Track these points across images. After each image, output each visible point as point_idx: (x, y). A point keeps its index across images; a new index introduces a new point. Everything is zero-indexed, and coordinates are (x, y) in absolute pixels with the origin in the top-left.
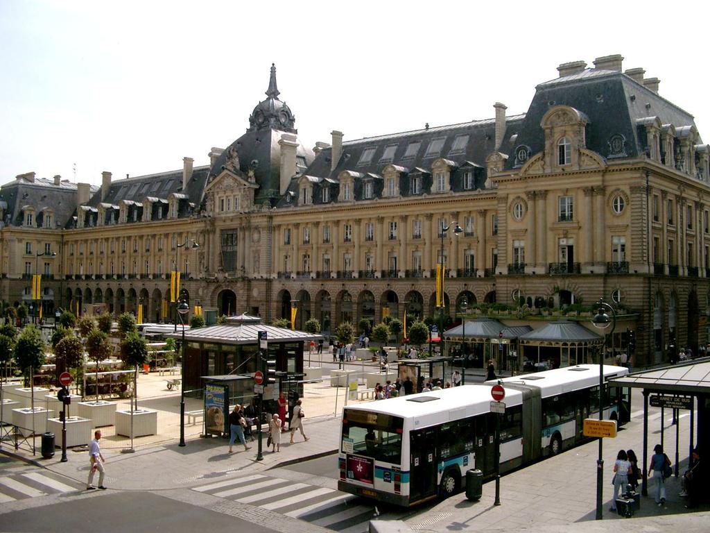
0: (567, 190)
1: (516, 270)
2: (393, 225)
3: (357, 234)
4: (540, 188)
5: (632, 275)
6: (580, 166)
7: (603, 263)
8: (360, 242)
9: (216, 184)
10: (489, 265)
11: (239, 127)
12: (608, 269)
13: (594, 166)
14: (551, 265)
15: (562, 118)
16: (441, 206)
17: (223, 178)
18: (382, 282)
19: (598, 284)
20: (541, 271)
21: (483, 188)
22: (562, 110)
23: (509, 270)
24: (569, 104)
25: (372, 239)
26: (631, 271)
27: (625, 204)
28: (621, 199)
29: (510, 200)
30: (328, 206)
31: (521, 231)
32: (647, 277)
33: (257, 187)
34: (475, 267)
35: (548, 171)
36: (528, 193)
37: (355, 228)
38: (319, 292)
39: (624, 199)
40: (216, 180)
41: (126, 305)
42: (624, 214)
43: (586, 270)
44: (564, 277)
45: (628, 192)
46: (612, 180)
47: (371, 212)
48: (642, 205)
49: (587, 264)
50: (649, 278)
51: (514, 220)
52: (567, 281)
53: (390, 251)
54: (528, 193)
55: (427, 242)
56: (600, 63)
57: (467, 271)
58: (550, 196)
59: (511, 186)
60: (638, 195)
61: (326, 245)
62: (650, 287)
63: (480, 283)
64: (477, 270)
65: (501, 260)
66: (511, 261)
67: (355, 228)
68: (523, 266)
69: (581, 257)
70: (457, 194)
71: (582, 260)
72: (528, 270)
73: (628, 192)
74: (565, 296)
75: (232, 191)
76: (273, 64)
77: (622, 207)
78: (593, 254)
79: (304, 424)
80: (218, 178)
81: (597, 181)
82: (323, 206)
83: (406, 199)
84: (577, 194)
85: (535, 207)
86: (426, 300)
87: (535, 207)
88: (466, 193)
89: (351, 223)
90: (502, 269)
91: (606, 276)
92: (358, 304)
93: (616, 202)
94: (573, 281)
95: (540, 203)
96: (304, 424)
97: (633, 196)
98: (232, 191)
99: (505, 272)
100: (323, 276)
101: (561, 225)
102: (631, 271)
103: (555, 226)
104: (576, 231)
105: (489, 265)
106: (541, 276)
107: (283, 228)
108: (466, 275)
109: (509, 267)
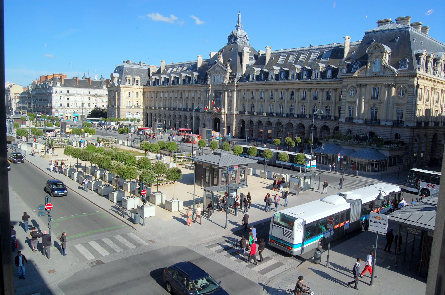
0: (377, 84)
1: (350, 120)
2: (304, 93)
3: (257, 96)
4: (363, 83)
5: (405, 127)
6: (384, 73)
7: (391, 121)
8: (323, 100)
9: (212, 69)
10: (337, 115)
11: (225, 42)
12: (394, 123)
13: (391, 74)
14: (366, 119)
15: (377, 49)
16: (316, 85)
17: (215, 66)
18: (287, 119)
19: (388, 131)
20: (361, 122)
21: (336, 78)
22: (377, 45)
23: (346, 120)
24: (381, 42)
25: (330, 99)
26: (405, 125)
27: (405, 93)
28: (403, 90)
29: (348, 87)
30: (263, 82)
31: (353, 102)
32: (413, 129)
33: (231, 71)
34: (378, 118)
35: (368, 74)
36: (357, 85)
37: (308, 93)
38: (277, 123)
39: (404, 90)
40: (212, 68)
41: (254, 130)
42: (404, 97)
43: (382, 123)
44: (372, 125)
45: (407, 87)
46: (399, 81)
47: (283, 86)
48: (413, 94)
49: (384, 120)
50: (414, 129)
51: (350, 96)
52: (373, 127)
53: (372, 106)
54: (357, 85)
55: (321, 101)
56: (398, 21)
57: (326, 116)
58: (368, 86)
59: (350, 81)
60: (412, 89)
61: (262, 100)
62: (413, 133)
63: (332, 122)
64: (331, 116)
65: (342, 115)
66: (347, 116)
67: (308, 93)
68: (353, 118)
69: (381, 116)
70: (324, 80)
71: (381, 118)
72: (355, 121)
73: (407, 87)
74: (371, 134)
75: (219, 73)
76: (102, 76)
77: (403, 95)
78: (387, 115)
79: (371, 221)
80: (213, 67)
81: (391, 81)
82: (261, 82)
83: (300, 81)
84: (381, 87)
85: (360, 91)
86: (306, 128)
87: (360, 91)
88: (328, 80)
89: (273, 90)
90: (342, 120)
91: (392, 127)
92: (285, 128)
93: (400, 92)
94: (376, 128)
95: (363, 89)
96: (371, 221)
97: (409, 89)
98: (219, 73)
99: (344, 120)
100: (279, 115)
101: (372, 101)
102: (405, 125)
103: (370, 101)
104: (379, 104)
105: (337, 115)
106: (360, 124)
107: (242, 91)
108: (279, 115)
109: (346, 118)
